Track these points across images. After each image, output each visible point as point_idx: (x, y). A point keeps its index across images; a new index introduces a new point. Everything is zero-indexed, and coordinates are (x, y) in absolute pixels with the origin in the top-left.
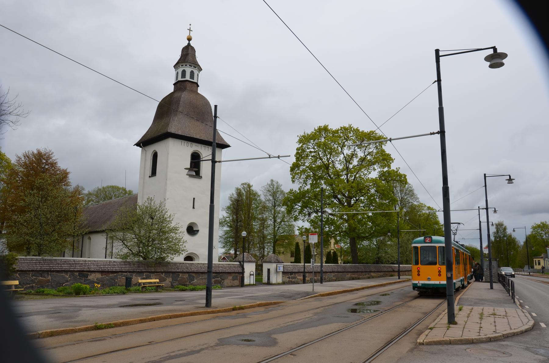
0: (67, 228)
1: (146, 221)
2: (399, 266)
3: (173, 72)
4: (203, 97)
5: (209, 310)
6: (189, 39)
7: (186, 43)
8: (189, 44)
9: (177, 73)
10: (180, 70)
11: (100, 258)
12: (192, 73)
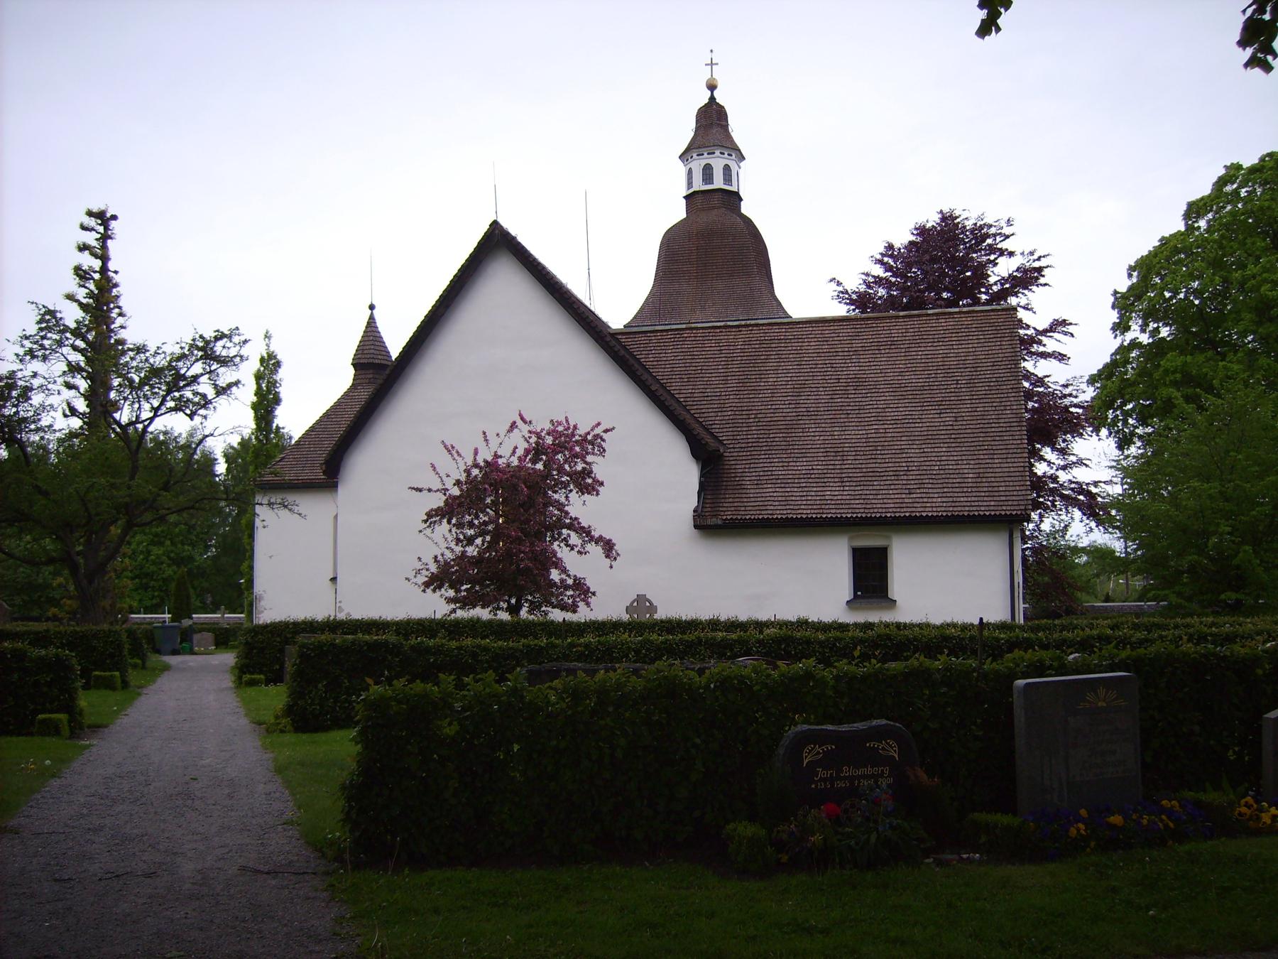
0: (1035, 348)
2: (870, 577)
3: (681, 170)
4: (748, 222)
5: (870, 541)
6: (712, 87)
7: (704, 100)
8: (712, 98)
9: (690, 172)
10: (697, 165)
12: (727, 169)
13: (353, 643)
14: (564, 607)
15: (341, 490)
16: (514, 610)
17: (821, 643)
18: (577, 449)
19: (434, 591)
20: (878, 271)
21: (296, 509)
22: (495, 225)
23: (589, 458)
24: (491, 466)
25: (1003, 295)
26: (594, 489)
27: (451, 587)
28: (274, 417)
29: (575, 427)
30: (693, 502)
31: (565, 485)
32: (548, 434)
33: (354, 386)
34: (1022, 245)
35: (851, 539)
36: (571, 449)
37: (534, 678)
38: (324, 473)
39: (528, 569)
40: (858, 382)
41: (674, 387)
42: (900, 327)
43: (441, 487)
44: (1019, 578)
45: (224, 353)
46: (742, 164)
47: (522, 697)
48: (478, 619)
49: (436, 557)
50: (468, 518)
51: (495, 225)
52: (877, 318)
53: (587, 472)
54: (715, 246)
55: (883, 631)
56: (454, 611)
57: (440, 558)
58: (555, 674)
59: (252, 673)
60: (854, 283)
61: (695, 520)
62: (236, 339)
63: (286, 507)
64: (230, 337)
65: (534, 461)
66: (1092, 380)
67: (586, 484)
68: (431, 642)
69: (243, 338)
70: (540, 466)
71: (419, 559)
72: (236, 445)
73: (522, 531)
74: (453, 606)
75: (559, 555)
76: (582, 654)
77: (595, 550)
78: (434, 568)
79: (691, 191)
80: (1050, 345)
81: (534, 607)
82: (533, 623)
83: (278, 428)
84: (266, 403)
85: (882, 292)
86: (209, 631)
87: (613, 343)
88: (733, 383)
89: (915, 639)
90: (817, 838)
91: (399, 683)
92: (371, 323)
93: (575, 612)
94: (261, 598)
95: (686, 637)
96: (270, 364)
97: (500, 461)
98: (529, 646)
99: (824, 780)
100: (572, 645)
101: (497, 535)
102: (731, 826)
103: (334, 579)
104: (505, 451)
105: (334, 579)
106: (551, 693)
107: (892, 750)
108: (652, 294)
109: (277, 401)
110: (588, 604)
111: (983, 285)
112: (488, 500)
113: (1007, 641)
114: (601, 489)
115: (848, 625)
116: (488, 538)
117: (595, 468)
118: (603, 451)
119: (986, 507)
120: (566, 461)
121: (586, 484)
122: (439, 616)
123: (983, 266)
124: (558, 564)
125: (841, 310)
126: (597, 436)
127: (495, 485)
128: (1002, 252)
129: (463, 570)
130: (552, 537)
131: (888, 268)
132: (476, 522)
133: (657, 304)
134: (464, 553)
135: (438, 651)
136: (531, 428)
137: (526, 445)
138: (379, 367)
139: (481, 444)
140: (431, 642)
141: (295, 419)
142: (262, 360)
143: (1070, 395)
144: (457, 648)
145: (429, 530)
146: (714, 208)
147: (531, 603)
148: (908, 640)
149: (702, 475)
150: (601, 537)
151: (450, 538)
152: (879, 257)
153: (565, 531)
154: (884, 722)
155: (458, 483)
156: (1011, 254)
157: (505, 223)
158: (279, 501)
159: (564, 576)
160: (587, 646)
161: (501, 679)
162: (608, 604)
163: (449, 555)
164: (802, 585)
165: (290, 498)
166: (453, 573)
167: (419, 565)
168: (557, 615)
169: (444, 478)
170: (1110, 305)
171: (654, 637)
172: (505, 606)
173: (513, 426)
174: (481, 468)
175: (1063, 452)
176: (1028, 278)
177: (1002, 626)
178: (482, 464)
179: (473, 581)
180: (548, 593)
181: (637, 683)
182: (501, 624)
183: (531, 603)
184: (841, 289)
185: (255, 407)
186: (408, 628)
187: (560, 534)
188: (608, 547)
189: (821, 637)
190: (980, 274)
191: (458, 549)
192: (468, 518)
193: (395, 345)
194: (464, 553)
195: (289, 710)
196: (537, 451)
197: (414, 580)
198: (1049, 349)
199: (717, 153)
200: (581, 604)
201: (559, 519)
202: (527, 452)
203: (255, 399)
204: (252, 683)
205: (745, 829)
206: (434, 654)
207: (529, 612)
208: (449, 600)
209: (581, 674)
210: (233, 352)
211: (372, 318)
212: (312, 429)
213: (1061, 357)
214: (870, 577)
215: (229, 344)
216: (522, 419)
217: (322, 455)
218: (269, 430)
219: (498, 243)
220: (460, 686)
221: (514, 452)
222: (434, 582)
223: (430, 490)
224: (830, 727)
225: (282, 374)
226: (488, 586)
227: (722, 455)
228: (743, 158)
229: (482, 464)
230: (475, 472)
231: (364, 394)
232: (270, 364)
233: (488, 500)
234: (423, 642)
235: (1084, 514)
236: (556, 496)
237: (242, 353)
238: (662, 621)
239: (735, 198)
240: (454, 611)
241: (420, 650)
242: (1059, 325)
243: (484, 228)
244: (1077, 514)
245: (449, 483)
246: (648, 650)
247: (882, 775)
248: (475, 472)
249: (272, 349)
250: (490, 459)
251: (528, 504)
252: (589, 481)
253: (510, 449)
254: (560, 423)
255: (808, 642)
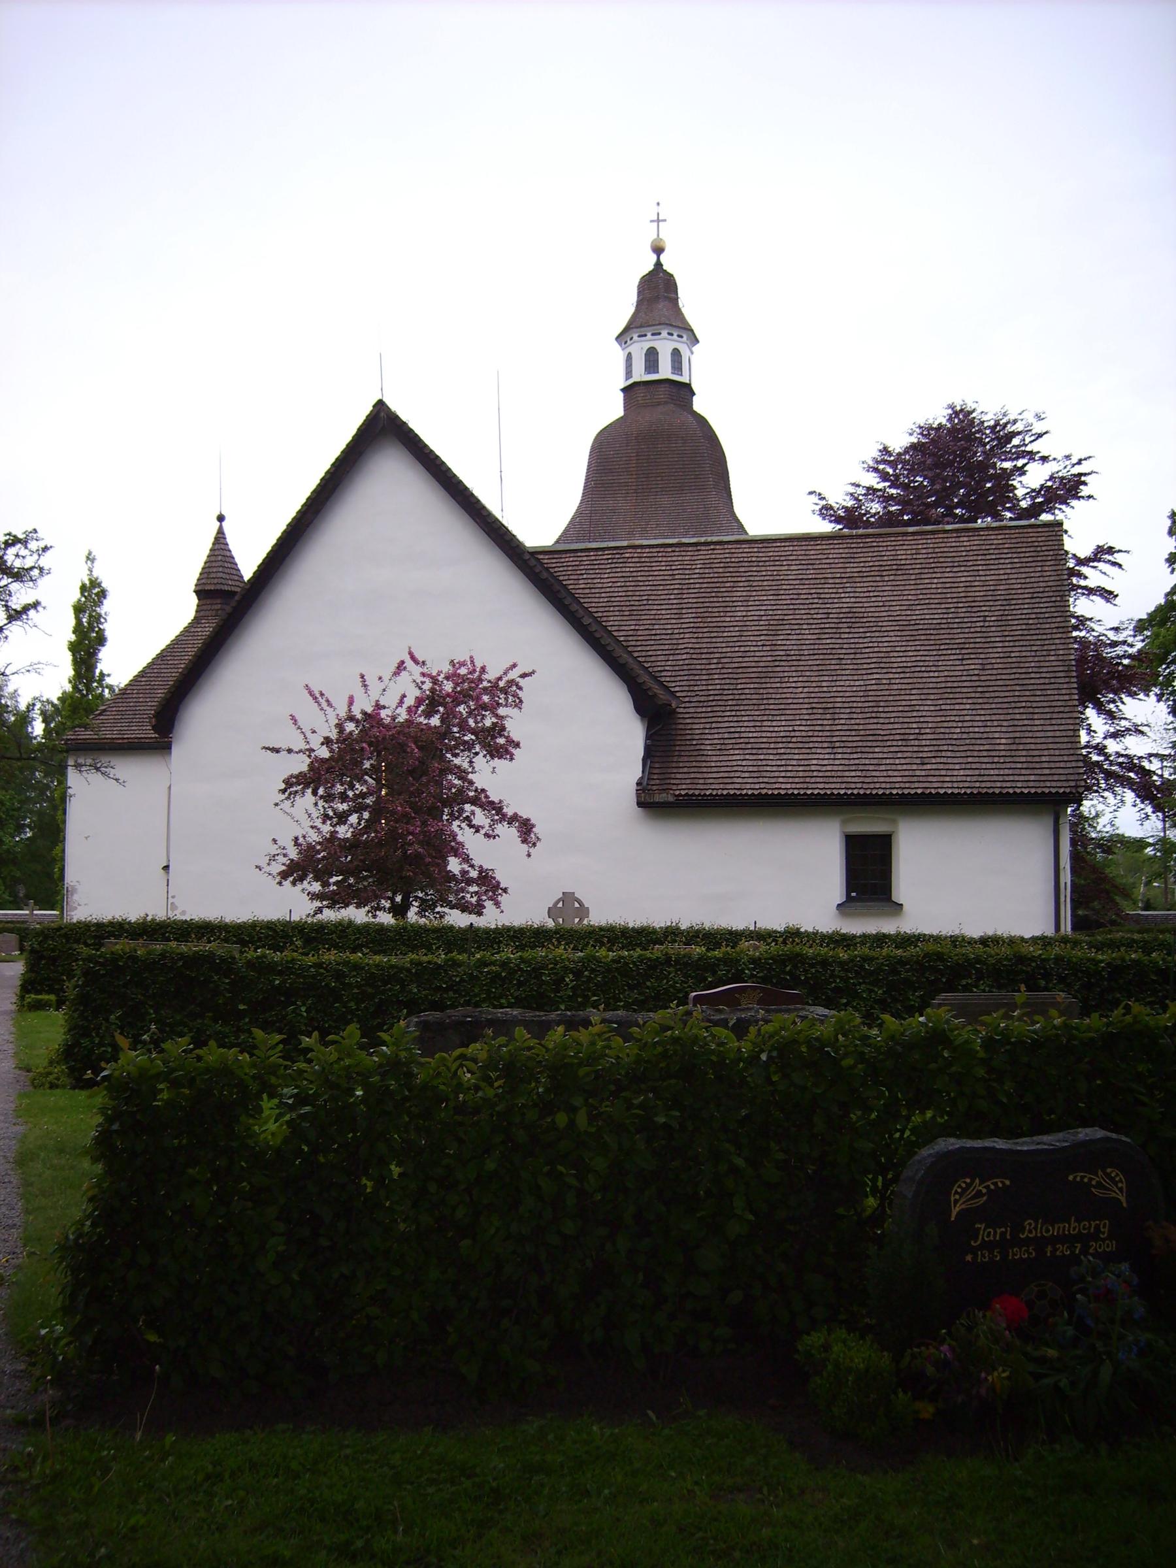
1: (287, 1554)
2: (869, 873)
3: (618, 355)
4: (702, 422)
6: (658, 250)
8: (658, 265)
9: (629, 358)
10: (639, 349)
11: (1155, 910)
12: (676, 354)
13: (163, 955)
14: (465, 908)
15: (178, 750)
16: (399, 911)
17: (842, 964)
18: (486, 698)
19: (294, 883)
20: (872, 480)
21: (112, 772)
22: (380, 405)
23: (502, 711)
24: (371, 718)
25: (1035, 510)
26: (507, 752)
27: (316, 879)
28: (97, 660)
29: (483, 670)
30: (636, 771)
31: (469, 746)
32: (447, 678)
33: (197, 620)
34: (1059, 445)
35: (844, 822)
36: (478, 698)
37: (431, 1037)
38: (154, 728)
39: (417, 856)
40: (853, 618)
41: (613, 622)
42: (906, 549)
43: (303, 746)
44: (1066, 877)
45: (18, 564)
46: (695, 349)
47: (410, 1075)
48: (350, 923)
49: (296, 839)
50: (339, 788)
51: (380, 405)
52: (880, 535)
53: (499, 729)
54: (658, 450)
55: (931, 947)
56: (319, 910)
57: (301, 840)
58: (470, 1032)
59: (38, 992)
60: (839, 498)
61: (638, 795)
62: (33, 545)
63: (97, 769)
64: (25, 542)
65: (428, 714)
66: (1140, 626)
67: (498, 745)
68: (277, 956)
69: (42, 544)
70: (435, 721)
71: (275, 841)
72: (56, 702)
73: (413, 806)
74: (318, 904)
75: (460, 838)
76: (497, 976)
77: (508, 833)
78: (293, 853)
79: (630, 381)
80: (1093, 577)
81: (426, 907)
82: (424, 930)
83: (102, 675)
84: (87, 644)
85: (876, 507)
86: (11, 931)
87: (533, 562)
88: (688, 617)
89: (978, 960)
90: (999, 1376)
91: (178, 1046)
92: (220, 539)
93: (480, 914)
94: (74, 890)
95: (648, 954)
96: (92, 596)
97: (383, 714)
98: (420, 963)
99: (988, 1246)
100: (483, 963)
101: (377, 811)
102: (815, 1339)
103: (166, 868)
104: (390, 700)
105: (166, 868)
106: (465, 1067)
107: (1114, 1186)
108: (579, 513)
109: (101, 640)
110: (497, 904)
111: (1009, 500)
112: (367, 765)
113: (1109, 964)
114: (515, 751)
115: (854, 936)
116: (366, 815)
117: (508, 724)
118: (518, 704)
119: (1022, 784)
120: (470, 713)
121: (498, 745)
122: (295, 918)
123: (1007, 475)
124: (458, 850)
125: (827, 527)
126: (511, 682)
127: (378, 746)
128: (1031, 455)
129: (332, 857)
130: (451, 814)
131: (884, 477)
132: (350, 794)
133: (587, 520)
134: (333, 834)
135: (287, 969)
136: (425, 670)
137: (418, 693)
138: (226, 595)
139: (358, 693)
140: (277, 956)
141: (120, 664)
142: (83, 588)
143: (1124, 642)
144: (315, 965)
145: (288, 803)
146: (659, 404)
147: (423, 901)
148: (968, 960)
149: (648, 737)
150: (516, 815)
151: (315, 814)
152: (871, 463)
153: (468, 807)
154: (1099, 1133)
155: (327, 741)
156: (1044, 459)
157: (394, 405)
158: (89, 761)
159: (466, 867)
160: (504, 964)
161: (371, 1041)
162: (522, 907)
163: (314, 837)
164: (772, 882)
165: (104, 759)
166: (319, 860)
167: (274, 850)
168: (458, 919)
169: (309, 734)
170: (1166, 530)
171: (602, 952)
172: (388, 905)
173: (401, 667)
174: (357, 722)
175: (1111, 716)
176: (1069, 488)
177: (1042, 941)
178: (359, 716)
179: (345, 871)
180: (445, 889)
181: (624, 1050)
182: (381, 929)
183: (423, 901)
184: (824, 502)
185: (74, 648)
186: (276, 934)
187: (461, 811)
188: (526, 829)
189: (843, 955)
190: (1003, 482)
191: (326, 828)
192: (339, 788)
193: (248, 567)
194: (333, 834)
195: (69, 1053)
196: (432, 701)
197: (267, 869)
198: (1091, 583)
199: (664, 333)
200: (489, 904)
201: (461, 791)
202: (419, 701)
203: (73, 638)
204: (38, 1006)
205: (851, 1352)
206: (280, 973)
207: (420, 913)
208: (314, 896)
209: (520, 1032)
210: (29, 563)
211: (221, 528)
212: (143, 674)
213: (1108, 595)
214: (869, 873)
215: (23, 552)
216: (413, 658)
217: (150, 706)
218: (91, 679)
219: (383, 430)
220: (293, 1051)
221: (401, 702)
222: (295, 872)
223: (290, 751)
224: (1000, 1144)
225: (107, 607)
226: (365, 878)
227: (674, 712)
228: (697, 341)
229: (359, 716)
230: (350, 727)
231: (208, 629)
232: (92, 596)
233: (367, 765)
234: (264, 956)
235: (1138, 796)
236: (457, 761)
237: (42, 563)
238: (601, 929)
239: (687, 390)
240: (319, 910)
241: (262, 967)
242: (1102, 553)
243: (367, 409)
244: (1129, 796)
245: (316, 742)
246: (593, 971)
247: (1095, 1236)
248: (350, 727)
249: (95, 574)
250: (369, 710)
251: (421, 770)
252: (501, 741)
253: (397, 698)
254: (462, 664)
255: (824, 963)
